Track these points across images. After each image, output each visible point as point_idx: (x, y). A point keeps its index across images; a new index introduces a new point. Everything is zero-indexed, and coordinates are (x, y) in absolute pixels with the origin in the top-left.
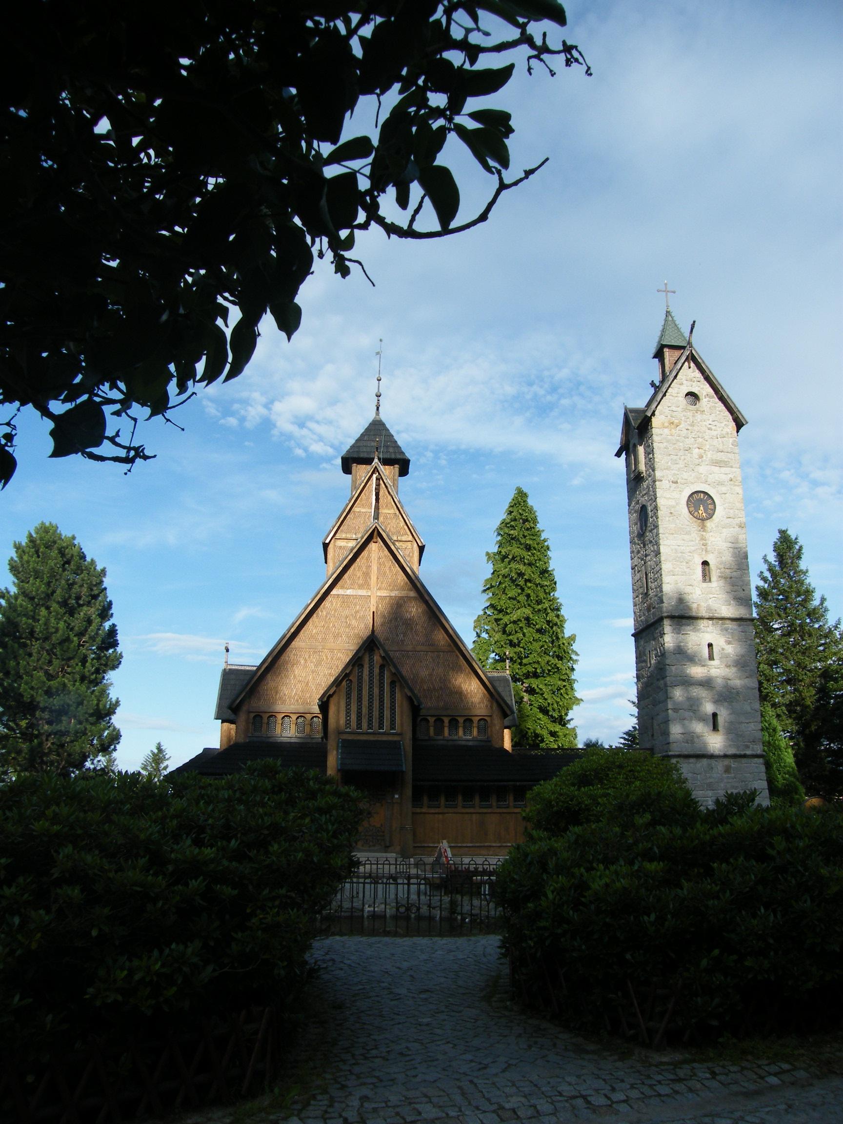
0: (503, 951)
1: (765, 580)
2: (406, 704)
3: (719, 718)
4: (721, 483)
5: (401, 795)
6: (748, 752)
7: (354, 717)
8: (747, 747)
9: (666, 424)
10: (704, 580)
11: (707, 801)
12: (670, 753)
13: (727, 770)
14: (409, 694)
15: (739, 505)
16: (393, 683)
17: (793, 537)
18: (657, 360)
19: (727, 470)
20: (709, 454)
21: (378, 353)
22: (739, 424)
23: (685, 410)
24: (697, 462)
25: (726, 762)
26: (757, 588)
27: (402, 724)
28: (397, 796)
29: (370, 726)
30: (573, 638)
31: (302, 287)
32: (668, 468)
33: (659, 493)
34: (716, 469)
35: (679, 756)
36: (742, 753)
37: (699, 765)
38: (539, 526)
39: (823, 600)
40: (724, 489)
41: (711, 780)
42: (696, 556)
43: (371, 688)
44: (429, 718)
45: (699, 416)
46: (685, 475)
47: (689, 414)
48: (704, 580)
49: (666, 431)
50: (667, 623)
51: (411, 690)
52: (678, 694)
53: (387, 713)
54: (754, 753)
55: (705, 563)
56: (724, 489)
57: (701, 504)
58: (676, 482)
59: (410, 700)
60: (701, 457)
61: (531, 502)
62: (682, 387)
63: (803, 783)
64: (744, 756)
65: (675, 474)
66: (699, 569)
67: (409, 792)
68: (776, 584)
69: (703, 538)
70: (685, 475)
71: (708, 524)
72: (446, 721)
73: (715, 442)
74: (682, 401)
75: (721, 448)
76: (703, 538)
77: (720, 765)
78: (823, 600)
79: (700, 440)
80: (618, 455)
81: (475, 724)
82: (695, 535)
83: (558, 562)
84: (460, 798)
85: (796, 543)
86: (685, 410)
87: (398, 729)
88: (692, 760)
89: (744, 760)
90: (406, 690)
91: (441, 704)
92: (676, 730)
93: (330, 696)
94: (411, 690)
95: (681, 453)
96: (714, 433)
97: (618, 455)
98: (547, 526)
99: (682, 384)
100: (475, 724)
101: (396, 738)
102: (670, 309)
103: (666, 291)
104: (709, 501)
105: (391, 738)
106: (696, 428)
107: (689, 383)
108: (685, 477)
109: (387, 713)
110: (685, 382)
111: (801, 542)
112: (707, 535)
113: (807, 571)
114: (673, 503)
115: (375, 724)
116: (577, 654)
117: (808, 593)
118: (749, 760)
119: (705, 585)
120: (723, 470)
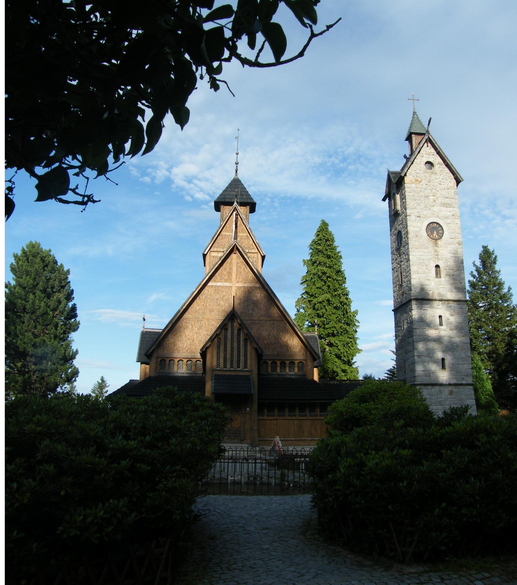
0: (313, 504)
1: (474, 276)
2: (254, 353)
3: (446, 361)
4: (447, 217)
5: (251, 408)
6: (464, 382)
7: (222, 361)
8: (463, 379)
9: (413, 181)
10: (437, 277)
11: (438, 412)
12: (416, 383)
13: (451, 393)
14: (256, 346)
15: (458, 231)
16: (246, 340)
17: (491, 250)
18: (408, 142)
19: (451, 209)
20: (440, 200)
21: (236, 138)
22: (458, 181)
23: (425, 172)
24: (432, 204)
25: (450, 388)
26: (469, 281)
27: (251, 365)
28: (248, 409)
29: (232, 366)
30: (356, 312)
31: (190, 97)
32: (415, 208)
33: (409, 223)
35: (421, 385)
36: (460, 383)
37: (433, 390)
39: (510, 289)
40: (448, 221)
42: (432, 262)
43: (232, 343)
44: (268, 361)
45: (433, 176)
46: (425, 213)
47: (428, 175)
48: (437, 277)
49: (413, 185)
50: (414, 303)
51: (257, 344)
52: (421, 346)
54: (467, 383)
55: (437, 266)
56: (448, 221)
57: (435, 230)
58: (420, 217)
59: (256, 350)
60: (435, 201)
61: (330, 229)
64: (461, 385)
65: (419, 212)
66: (434, 270)
67: (255, 406)
68: (480, 279)
69: (436, 251)
70: (425, 213)
71: (439, 242)
72: (279, 363)
73: (443, 192)
74: (423, 167)
75: (447, 196)
76: (436, 251)
77: (446, 390)
78: (510, 289)
79: (434, 191)
80: (384, 200)
81: (296, 365)
82: (431, 249)
83: (347, 266)
84: (287, 410)
85: (493, 254)
86: (425, 172)
87: (249, 368)
88: (429, 387)
89: (461, 387)
90: (254, 344)
91: (276, 353)
92: (419, 369)
93: (207, 348)
94: (257, 344)
96: (443, 187)
97: (384, 200)
98: (341, 244)
99: (423, 156)
100: (296, 365)
101: (248, 374)
102: (416, 111)
103: (413, 100)
104: (440, 228)
105: (244, 374)
106: (431, 184)
107: (427, 156)
108: (425, 214)
109: (242, 358)
111: (496, 253)
112: (438, 249)
113: (500, 271)
114: (417, 229)
115: (235, 365)
116: (359, 322)
117: (500, 285)
118: (464, 387)
119: (437, 280)
120: (448, 209)
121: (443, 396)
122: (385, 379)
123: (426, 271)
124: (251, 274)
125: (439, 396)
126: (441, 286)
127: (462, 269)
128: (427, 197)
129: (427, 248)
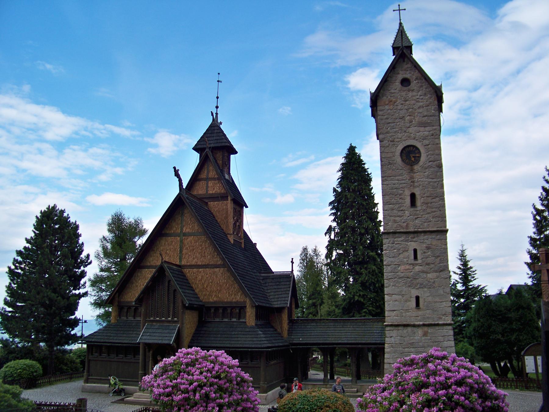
3: (420, 299)
6: (440, 322)
13: (425, 334)
20: (417, 119)
24: (408, 125)
25: (426, 329)
34: (422, 129)
35: (391, 325)
37: (405, 331)
40: (427, 142)
45: (410, 94)
46: (400, 135)
58: (393, 141)
60: (411, 122)
61: (357, 151)
64: (438, 325)
66: (408, 200)
71: (416, 167)
76: (412, 178)
77: (420, 331)
82: (406, 176)
88: (400, 328)
89: (437, 328)
95: (397, 121)
96: (421, 104)
114: (390, 155)
118: (442, 328)
119: (412, 209)
128: (403, 118)
129: (401, 175)
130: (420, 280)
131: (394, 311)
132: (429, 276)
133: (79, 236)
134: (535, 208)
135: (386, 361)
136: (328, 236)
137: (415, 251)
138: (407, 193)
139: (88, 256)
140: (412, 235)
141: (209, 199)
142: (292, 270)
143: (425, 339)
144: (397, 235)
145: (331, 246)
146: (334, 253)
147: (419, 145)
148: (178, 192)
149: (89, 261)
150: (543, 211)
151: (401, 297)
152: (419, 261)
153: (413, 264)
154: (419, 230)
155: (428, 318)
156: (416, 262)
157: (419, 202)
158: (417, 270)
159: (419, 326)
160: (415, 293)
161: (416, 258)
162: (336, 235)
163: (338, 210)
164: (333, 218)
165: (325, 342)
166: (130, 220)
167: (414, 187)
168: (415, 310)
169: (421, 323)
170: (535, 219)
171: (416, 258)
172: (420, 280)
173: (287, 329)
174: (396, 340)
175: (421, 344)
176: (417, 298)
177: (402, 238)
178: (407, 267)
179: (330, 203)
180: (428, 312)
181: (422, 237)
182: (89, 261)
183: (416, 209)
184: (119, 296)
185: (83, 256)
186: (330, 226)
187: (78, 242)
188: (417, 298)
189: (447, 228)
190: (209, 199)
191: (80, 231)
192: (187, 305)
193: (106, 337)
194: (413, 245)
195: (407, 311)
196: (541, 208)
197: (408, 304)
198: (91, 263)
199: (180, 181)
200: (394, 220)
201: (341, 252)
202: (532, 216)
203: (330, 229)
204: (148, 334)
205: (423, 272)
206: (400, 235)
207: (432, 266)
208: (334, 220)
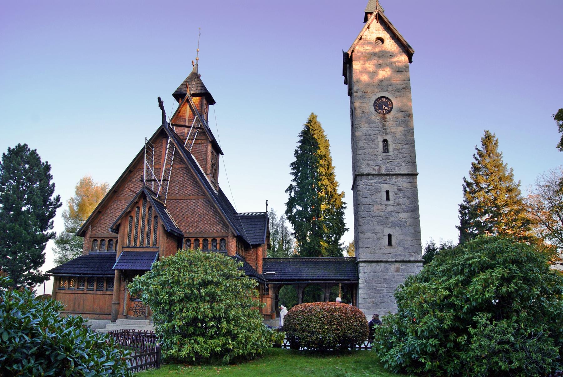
3: (392, 237)
6: (412, 259)
7: (133, 238)
10: (384, 152)
11: (383, 290)
13: (397, 270)
25: (397, 265)
35: (365, 262)
36: (408, 259)
37: (378, 267)
38: (325, 134)
39: (512, 169)
41: (387, 277)
42: (379, 137)
43: (144, 221)
44: (191, 239)
48: (384, 152)
53: (152, 235)
54: (416, 259)
61: (318, 120)
62: (372, 35)
63: (525, 284)
64: (410, 261)
66: (381, 145)
72: (201, 240)
76: (384, 126)
77: (393, 267)
78: (512, 169)
85: (494, 137)
88: (373, 264)
89: (409, 264)
93: (120, 225)
99: (373, 33)
104: (389, 102)
107: (377, 32)
109: (152, 235)
110: (375, 31)
118: (413, 264)
119: (384, 154)
121: (389, 274)
122: (42, 251)
123: (373, 146)
124: (404, 179)
125: (384, 274)
126: (388, 161)
127: (412, 142)
130: (392, 220)
131: (368, 248)
132: (401, 215)
133: (51, 177)
134: (465, 181)
135: (360, 296)
136: (288, 193)
137: (387, 192)
138: (380, 139)
139: (58, 199)
140: (384, 178)
141: (184, 142)
142: (267, 211)
143: (397, 275)
144: (370, 177)
145: (291, 204)
146: (294, 210)
147: (374, 98)
148: (161, 124)
149: (59, 203)
150: (472, 184)
151: (374, 235)
152: (391, 202)
153: (385, 205)
154: (392, 173)
155: (400, 255)
156: (388, 202)
157: (391, 147)
158: (389, 210)
159: (391, 262)
160: (387, 231)
161: (388, 199)
162: (296, 193)
163: (298, 171)
164: (293, 177)
165: (300, 278)
166: (98, 185)
167: (386, 134)
168: (388, 247)
169: (394, 260)
170: (465, 190)
171: (388, 199)
172: (392, 220)
173: (262, 265)
174: (370, 275)
175: (394, 280)
176: (390, 236)
177: (375, 181)
178: (380, 207)
179: (292, 164)
180: (400, 249)
181: (394, 179)
182: (59, 203)
183: (388, 154)
184: (92, 227)
185: (53, 198)
186: (291, 185)
187: (48, 185)
188: (390, 236)
189: (417, 172)
190: (184, 142)
191: (51, 172)
192: (169, 231)
193: (77, 269)
194: (386, 187)
195: (380, 248)
196: (470, 180)
197: (380, 241)
198: (60, 205)
199: (164, 113)
200: (368, 164)
201: (301, 209)
202: (462, 188)
203: (291, 188)
204: (125, 261)
205: (396, 212)
206: (373, 177)
207: (404, 206)
208: (294, 180)
